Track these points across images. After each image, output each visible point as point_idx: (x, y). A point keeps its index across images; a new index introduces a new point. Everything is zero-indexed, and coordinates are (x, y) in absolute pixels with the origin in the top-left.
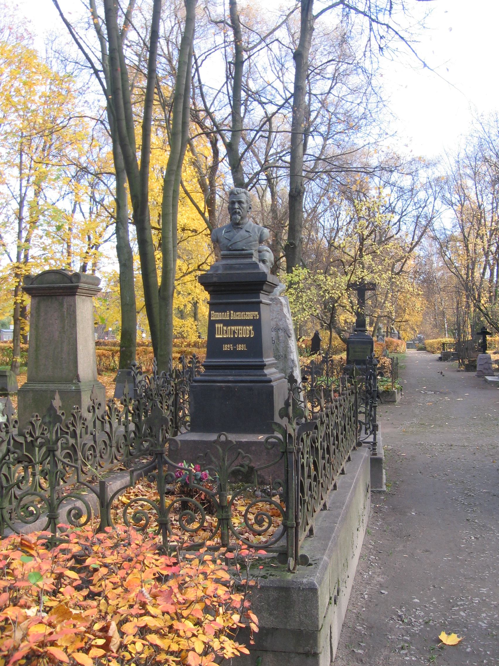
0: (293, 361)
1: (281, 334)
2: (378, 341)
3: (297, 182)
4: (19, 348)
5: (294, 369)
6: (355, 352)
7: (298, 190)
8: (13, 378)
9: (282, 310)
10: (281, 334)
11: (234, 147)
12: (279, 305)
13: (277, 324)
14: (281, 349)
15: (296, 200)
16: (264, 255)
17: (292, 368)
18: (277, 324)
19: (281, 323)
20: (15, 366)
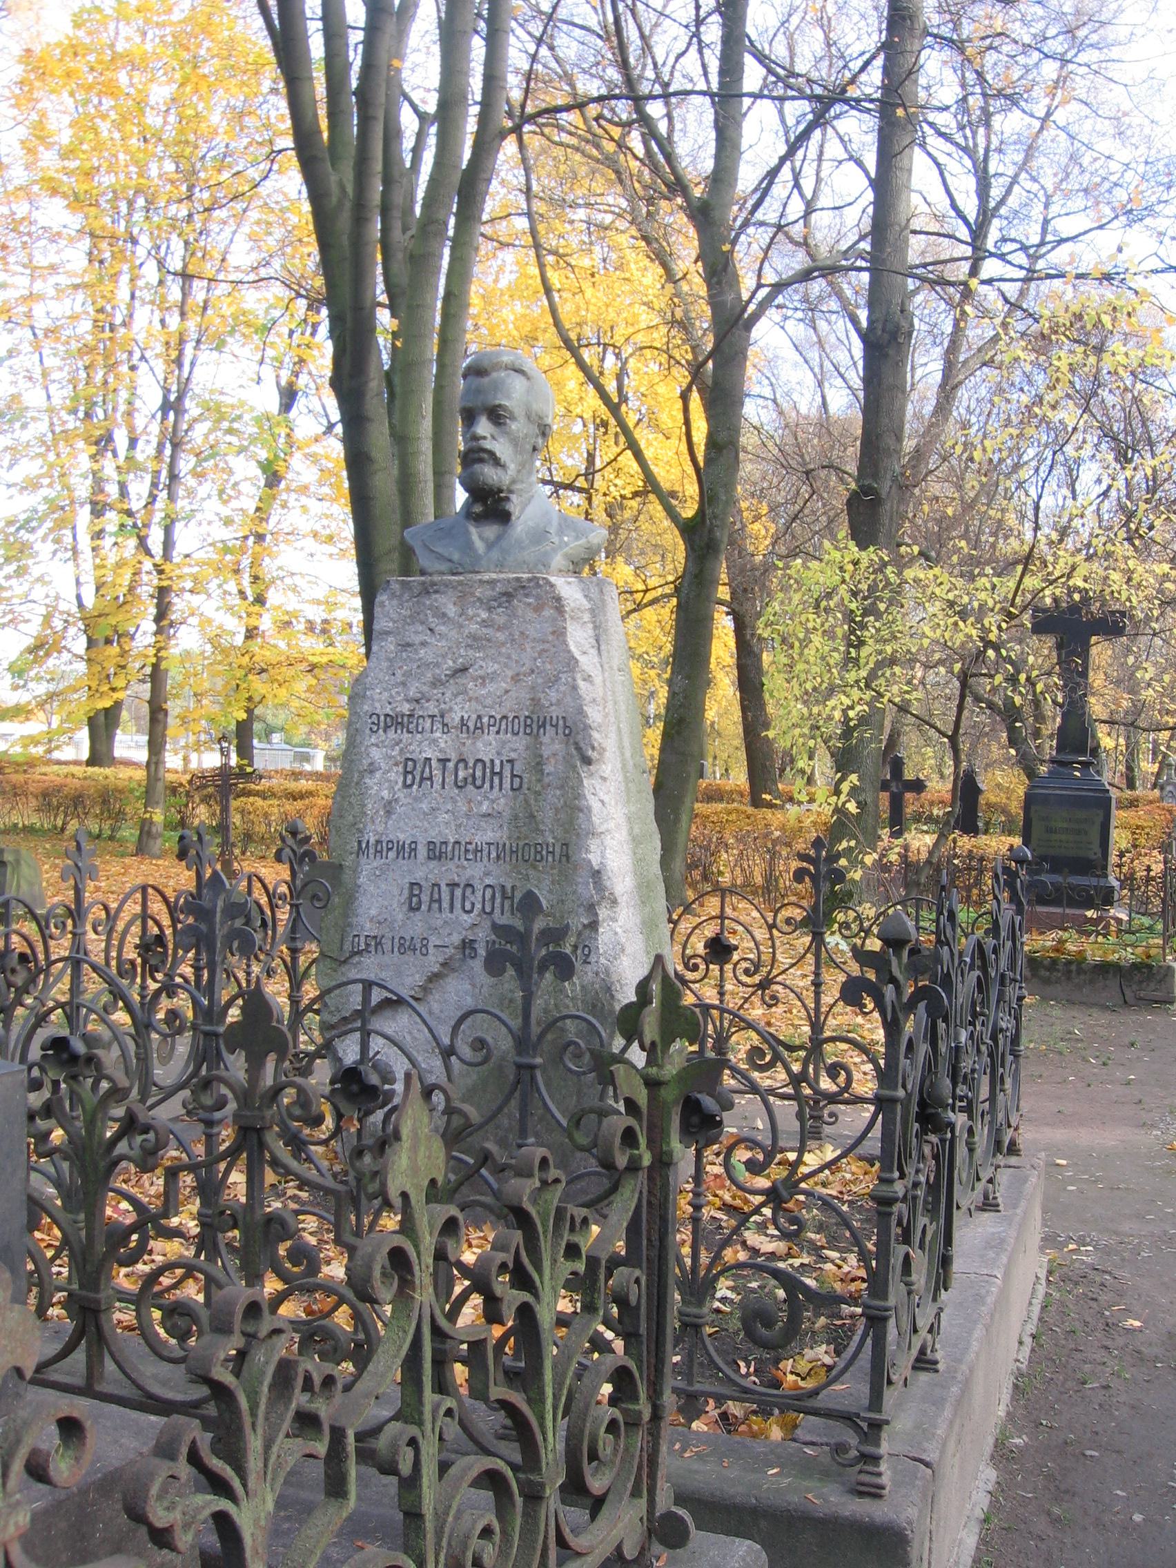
0: (597, 874)
1: (552, 744)
2: (1162, 799)
3: (889, 302)
4: (160, 785)
5: (603, 913)
6: (1049, 830)
7: (889, 327)
8: (25, 870)
9: (560, 634)
10: (552, 744)
11: (716, 214)
12: (548, 612)
13: (535, 701)
14: (547, 816)
15: (886, 356)
16: (497, 387)
17: (591, 908)
18: (535, 701)
19: (553, 695)
20: (149, 833)
